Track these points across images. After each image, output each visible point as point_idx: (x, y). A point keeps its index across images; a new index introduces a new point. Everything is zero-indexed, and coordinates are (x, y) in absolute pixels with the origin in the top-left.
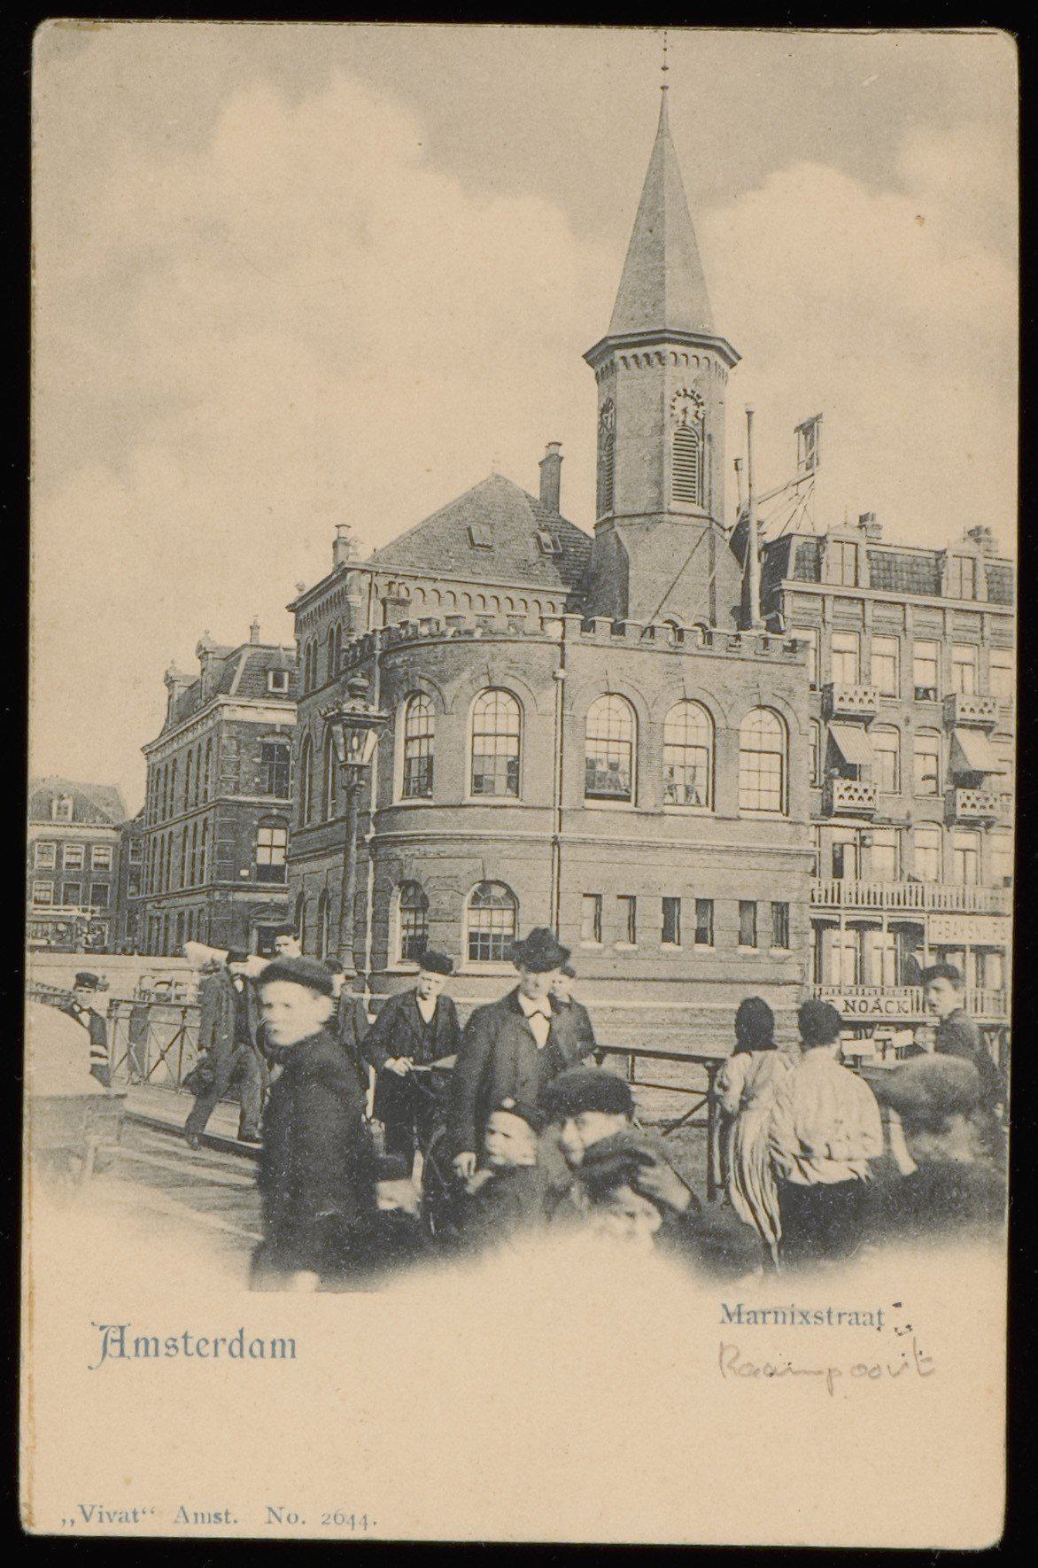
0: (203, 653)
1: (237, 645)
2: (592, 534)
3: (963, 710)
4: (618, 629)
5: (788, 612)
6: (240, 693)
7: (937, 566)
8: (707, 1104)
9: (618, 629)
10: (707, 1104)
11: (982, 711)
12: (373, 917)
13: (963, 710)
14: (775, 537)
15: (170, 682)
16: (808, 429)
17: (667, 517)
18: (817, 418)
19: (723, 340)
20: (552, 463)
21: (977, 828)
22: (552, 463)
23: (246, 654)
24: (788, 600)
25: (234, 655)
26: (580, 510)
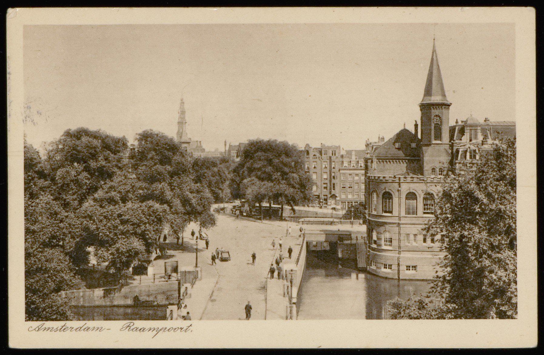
8: (413, 132)
10: (413, 132)
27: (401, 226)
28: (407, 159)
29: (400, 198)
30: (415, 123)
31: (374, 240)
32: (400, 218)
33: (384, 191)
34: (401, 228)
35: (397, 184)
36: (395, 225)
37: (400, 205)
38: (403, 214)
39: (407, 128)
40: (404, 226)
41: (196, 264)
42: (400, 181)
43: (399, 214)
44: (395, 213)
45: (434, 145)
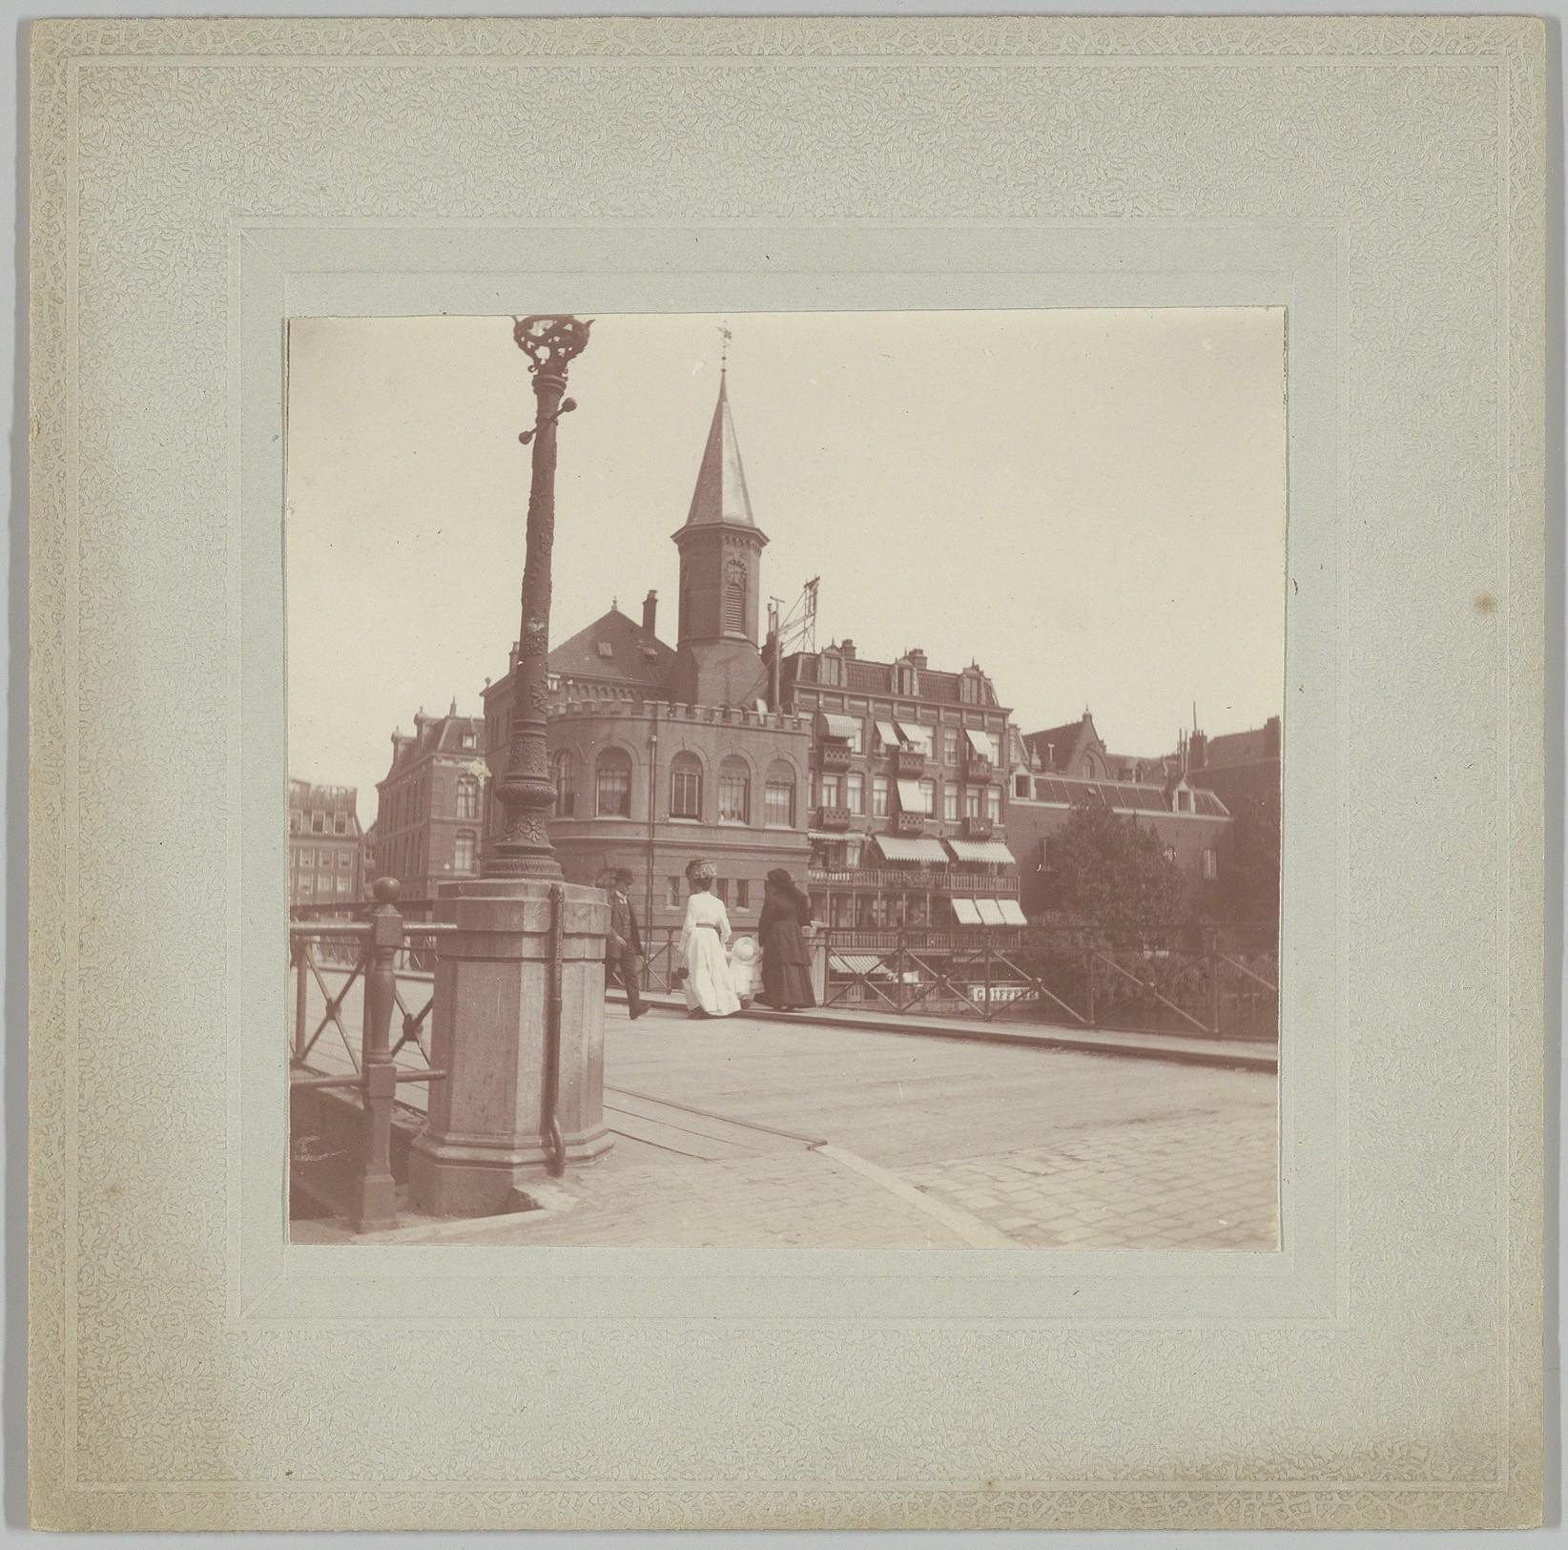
0: (419, 721)
1: (443, 717)
2: (676, 649)
3: (828, 816)
4: (689, 711)
5: (796, 701)
6: (443, 751)
7: (888, 673)
8: (639, 621)
9: (689, 711)
10: (639, 621)
11: (835, 817)
12: (517, 902)
13: (828, 816)
14: (790, 654)
15: (395, 740)
16: (811, 585)
17: (722, 641)
18: (817, 579)
19: (758, 530)
20: (650, 604)
21: (640, 909)
22: (650, 604)
23: (449, 723)
24: (796, 693)
25: (441, 723)
26: (668, 631)
27: (657, 852)
28: (634, 686)
29: (653, 767)
30: (451, 702)
31: (888, 746)
32: (651, 826)
33: (605, 745)
34: (656, 859)
35: (647, 724)
36: (637, 850)
37: (653, 787)
38: (662, 812)
39: (622, 609)
40: (667, 852)
41: (549, 385)
42: (656, 715)
43: (652, 813)
44: (641, 811)
45: (727, 642)
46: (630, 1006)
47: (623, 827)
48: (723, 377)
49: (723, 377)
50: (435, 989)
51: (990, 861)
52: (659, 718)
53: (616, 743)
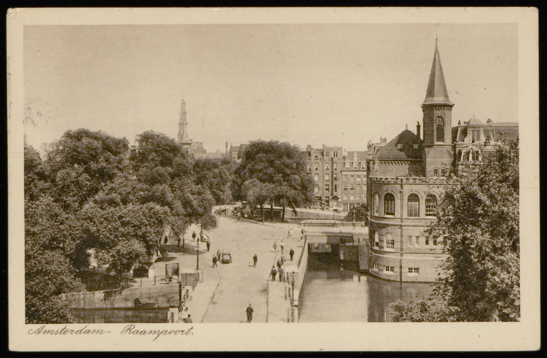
8: (416, 133)
10: (416, 133)
17: (435, 146)
27: (403, 228)
29: (402, 200)
32: (402, 220)
33: (386, 192)
37: (402, 207)
38: (405, 215)
39: (410, 129)
42: (402, 182)
44: (398, 214)
46: (9, 7)
47: (391, 220)
48: (436, 43)
49: (436, 43)
50: (13, 6)
51: (294, 225)
52: (403, 183)
53: (389, 192)
